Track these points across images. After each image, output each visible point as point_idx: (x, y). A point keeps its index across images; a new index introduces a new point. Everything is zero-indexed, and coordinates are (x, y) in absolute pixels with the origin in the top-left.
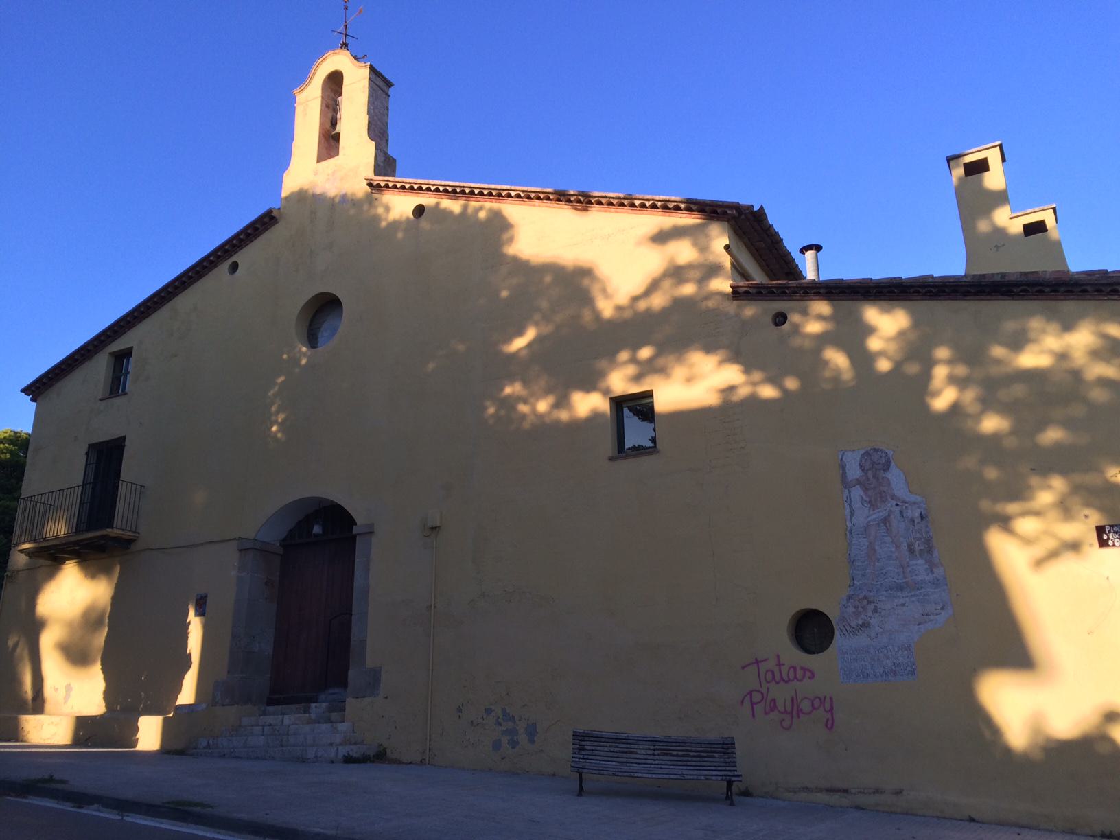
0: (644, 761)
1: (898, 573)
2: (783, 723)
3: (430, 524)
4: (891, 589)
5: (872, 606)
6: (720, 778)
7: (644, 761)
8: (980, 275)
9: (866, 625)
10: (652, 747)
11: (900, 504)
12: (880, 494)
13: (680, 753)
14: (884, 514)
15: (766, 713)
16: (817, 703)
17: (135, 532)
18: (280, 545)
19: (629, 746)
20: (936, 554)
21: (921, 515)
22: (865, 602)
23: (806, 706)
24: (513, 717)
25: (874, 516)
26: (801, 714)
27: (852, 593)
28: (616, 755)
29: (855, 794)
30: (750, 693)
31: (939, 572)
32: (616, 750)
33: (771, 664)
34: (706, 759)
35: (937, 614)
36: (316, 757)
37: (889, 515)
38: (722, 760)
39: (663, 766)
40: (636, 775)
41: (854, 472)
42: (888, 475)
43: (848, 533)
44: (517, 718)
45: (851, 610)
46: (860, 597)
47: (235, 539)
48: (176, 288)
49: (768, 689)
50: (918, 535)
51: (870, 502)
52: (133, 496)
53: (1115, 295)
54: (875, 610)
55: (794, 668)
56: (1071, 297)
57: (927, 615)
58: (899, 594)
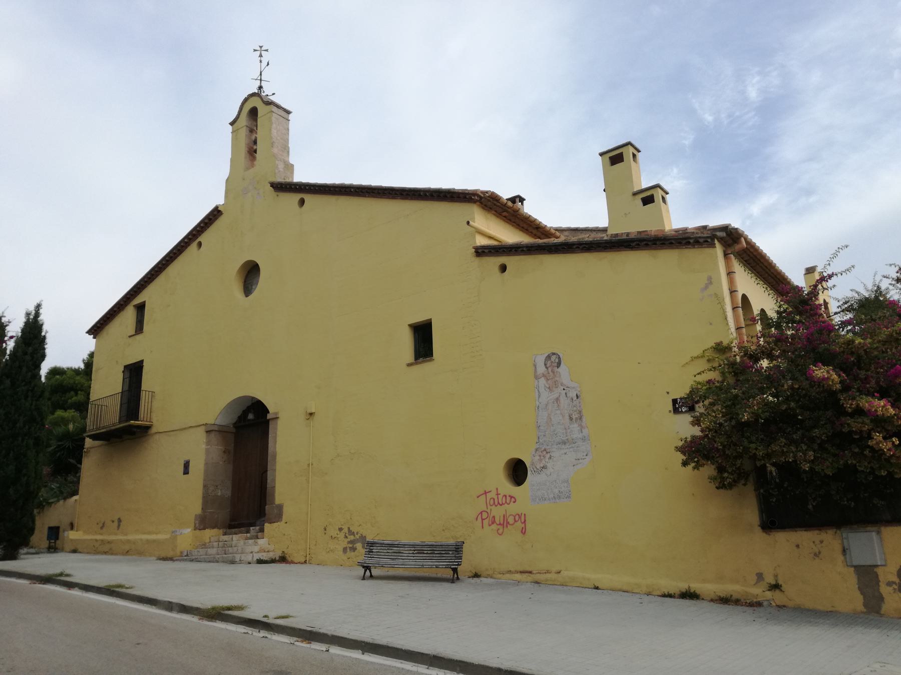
0: (406, 558)
1: (563, 433)
2: (499, 531)
3: (309, 411)
4: (560, 444)
5: (548, 456)
6: (444, 566)
7: (406, 558)
8: (615, 234)
9: (544, 467)
10: (412, 549)
11: (565, 388)
12: (555, 382)
13: (429, 552)
14: (556, 396)
15: (490, 525)
16: (517, 519)
17: (150, 422)
18: (233, 427)
19: (398, 549)
20: (584, 420)
21: (577, 395)
22: (545, 453)
23: (511, 520)
24: (354, 532)
25: (551, 397)
26: (508, 525)
27: (538, 447)
28: (390, 554)
29: (536, 574)
30: (481, 513)
31: (585, 431)
32: (390, 551)
33: (493, 495)
34: (444, 555)
35: (584, 459)
36: (240, 560)
37: (559, 396)
38: (453, 555)
39: (417, 560)
40: (395, 566)
41: (541, 369)
42: (559, 370)
43: (537, 408)
44: (355, 533)
45: (537, 458)
46: (542, 450)
47: (203, 425)
48: (167, 261)
49: (491, 510)
50: (575, 408)
51: (549, 388)
52: (147, 398)
53: (688, 245)
54: (550, 458)
55: (506, 496)
56: (665, 247)
57: (578, 460)
58: (563, 446)
